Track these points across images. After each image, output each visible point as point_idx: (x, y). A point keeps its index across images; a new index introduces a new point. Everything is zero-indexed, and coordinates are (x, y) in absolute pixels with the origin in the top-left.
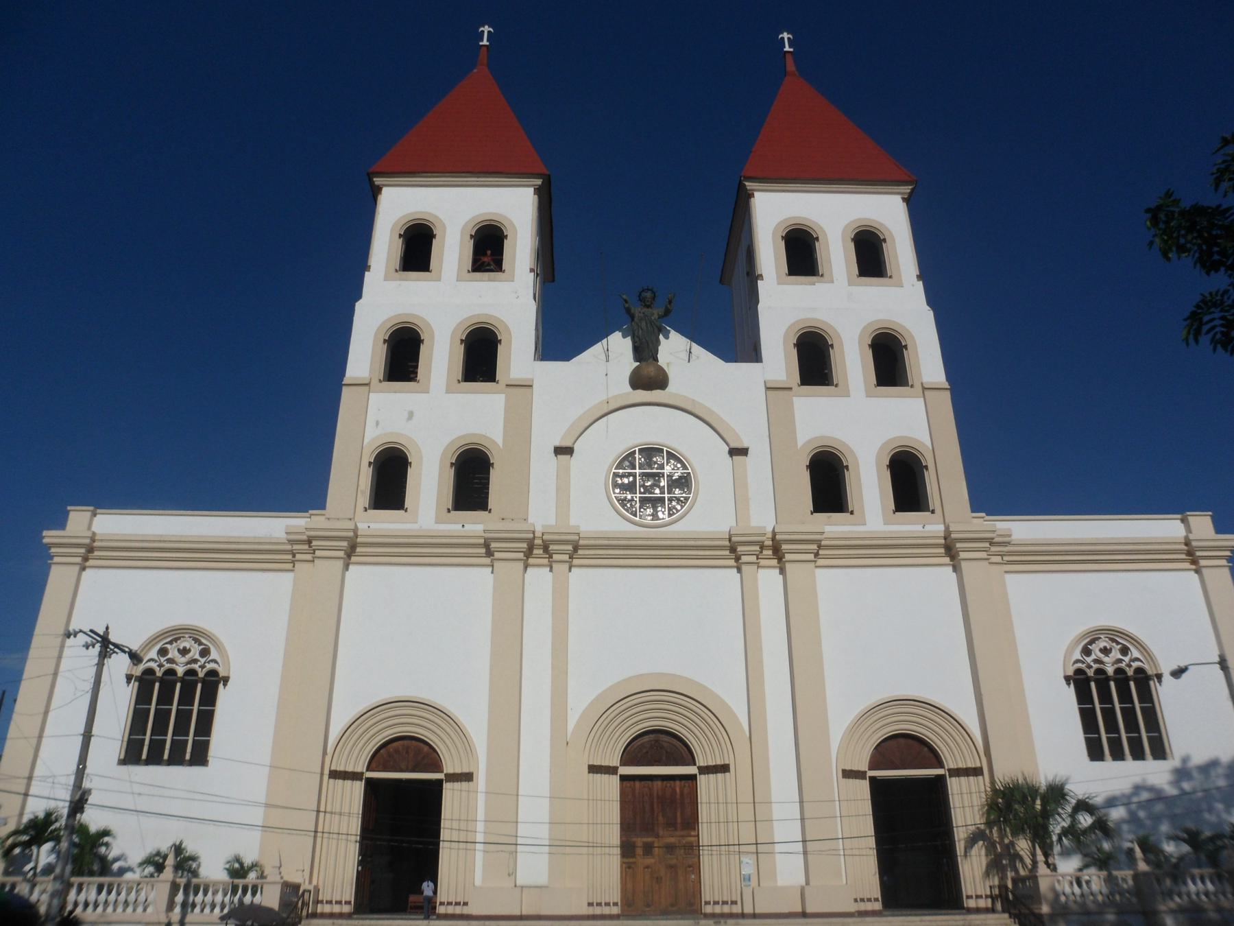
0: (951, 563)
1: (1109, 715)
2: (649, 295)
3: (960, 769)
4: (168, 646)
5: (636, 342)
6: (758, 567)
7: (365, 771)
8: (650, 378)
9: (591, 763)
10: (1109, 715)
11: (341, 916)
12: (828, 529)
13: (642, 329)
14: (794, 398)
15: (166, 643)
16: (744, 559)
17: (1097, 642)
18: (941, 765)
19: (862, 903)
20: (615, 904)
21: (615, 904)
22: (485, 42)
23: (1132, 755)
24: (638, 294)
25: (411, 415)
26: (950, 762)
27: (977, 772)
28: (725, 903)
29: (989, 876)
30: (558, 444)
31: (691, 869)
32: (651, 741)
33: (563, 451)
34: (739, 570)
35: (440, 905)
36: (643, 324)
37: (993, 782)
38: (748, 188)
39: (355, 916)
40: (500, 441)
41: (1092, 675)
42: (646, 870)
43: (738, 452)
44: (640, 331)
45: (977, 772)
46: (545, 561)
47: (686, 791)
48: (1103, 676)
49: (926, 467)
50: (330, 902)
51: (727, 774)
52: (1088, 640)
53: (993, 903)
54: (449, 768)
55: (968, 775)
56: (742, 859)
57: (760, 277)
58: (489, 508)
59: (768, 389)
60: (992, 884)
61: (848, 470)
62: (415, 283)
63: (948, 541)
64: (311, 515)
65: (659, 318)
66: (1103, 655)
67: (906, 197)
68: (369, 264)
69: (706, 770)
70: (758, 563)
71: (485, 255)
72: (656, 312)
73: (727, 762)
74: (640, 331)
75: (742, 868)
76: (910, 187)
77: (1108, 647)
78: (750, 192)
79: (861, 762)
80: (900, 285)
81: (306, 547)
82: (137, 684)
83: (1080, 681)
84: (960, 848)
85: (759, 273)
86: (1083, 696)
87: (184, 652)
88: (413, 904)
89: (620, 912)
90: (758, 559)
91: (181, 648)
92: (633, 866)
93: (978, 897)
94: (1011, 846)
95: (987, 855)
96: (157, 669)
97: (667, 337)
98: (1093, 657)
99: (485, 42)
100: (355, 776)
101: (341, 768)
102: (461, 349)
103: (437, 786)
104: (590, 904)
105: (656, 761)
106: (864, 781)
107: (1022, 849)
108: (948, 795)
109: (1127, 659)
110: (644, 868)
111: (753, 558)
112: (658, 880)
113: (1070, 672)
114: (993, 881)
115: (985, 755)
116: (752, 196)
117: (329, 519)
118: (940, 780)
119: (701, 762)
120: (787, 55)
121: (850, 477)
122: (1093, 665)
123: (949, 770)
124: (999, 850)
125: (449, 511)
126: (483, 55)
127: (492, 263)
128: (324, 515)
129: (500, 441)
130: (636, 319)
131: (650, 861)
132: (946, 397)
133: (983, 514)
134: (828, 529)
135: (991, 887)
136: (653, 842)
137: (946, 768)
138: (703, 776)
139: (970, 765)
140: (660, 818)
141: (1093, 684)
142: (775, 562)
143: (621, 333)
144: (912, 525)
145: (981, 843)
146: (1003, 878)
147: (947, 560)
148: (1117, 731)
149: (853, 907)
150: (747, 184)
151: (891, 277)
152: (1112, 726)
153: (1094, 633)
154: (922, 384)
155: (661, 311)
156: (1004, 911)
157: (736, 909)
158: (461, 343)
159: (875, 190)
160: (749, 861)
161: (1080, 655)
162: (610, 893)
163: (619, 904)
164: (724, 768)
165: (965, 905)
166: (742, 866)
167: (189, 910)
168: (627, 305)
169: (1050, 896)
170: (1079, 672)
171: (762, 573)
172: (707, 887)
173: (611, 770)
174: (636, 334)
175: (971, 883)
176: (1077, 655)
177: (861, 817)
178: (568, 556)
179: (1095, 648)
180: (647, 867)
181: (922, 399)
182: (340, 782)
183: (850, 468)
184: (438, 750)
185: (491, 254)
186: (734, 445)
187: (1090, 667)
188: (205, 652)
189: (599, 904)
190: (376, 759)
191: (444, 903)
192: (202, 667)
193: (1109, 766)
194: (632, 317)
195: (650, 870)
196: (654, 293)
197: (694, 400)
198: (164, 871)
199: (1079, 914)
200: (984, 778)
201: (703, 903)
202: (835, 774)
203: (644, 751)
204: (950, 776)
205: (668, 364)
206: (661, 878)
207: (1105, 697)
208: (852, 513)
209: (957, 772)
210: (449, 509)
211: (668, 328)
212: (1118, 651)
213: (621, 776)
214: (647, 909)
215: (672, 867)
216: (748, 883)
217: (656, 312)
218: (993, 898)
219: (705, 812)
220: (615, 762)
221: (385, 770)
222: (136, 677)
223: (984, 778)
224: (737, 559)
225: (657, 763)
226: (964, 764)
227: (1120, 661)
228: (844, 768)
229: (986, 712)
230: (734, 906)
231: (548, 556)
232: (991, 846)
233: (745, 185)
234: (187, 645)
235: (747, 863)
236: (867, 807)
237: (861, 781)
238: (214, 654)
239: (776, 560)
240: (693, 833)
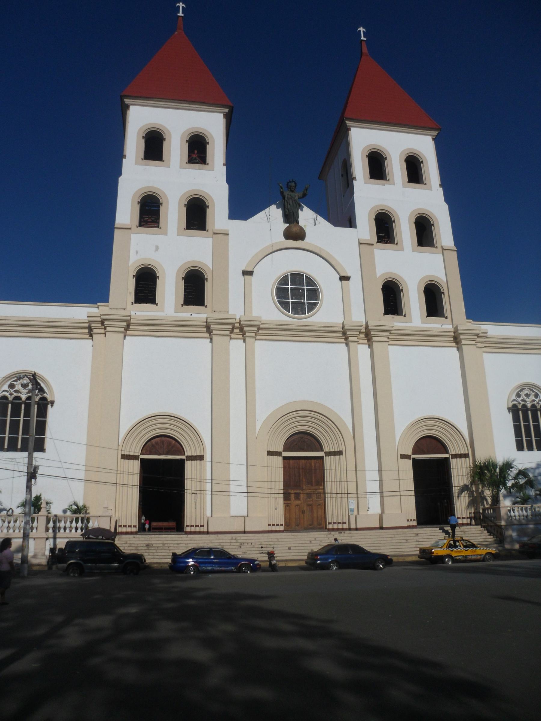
0: (368, 343)
1: (527, 428)
2: (293, 184)
3: (458, 454)
5: (286, 212)
6: (256, 340)
8: (297, 234)
9: (268, 450)
10: (527, 428)
11: (131, 533)
12: (396, 324)
13: (289, 204)
14: (375, 250)
16: (351, 339)
17: (523, 391)
18: (447, 452)
20: (282, 525)
21: (282, 525)
22: (180, 14)
23: (527, 448)
24: (286, 183)
25: (157, 248)
26: (453, 451)
27: (466, 456)
28: (339, 523)
29: (469, 508)
30: (244, 268)
31: (320, 506)
32: (298, 438)
33: (247, 273)
34: (244, 341)
35: (186, 527)
36: (291, 202)
38: (348, 125)
39: (139, 533)
41: (521, 408)
43: (344, 278)
44: (289, 206)
45: (466, 456)
46: (207, 335)
47: (317, 465)
48: (516, 408)
49: (443, 293)
51: (341, 456)
52: (519, 389)
53: (471, 520)
54: (189, 452)
55: (335, 455)
56: (349, 501)
57: (354, 178)
58: (156, 303)
59: (360, 244)
60: (470, 512)
62: (153, 167)
63: (456, 334)
64: (98, 306)
65: (298, 199)
66: (526, 398)
67: (434, 137)
68: (124, 154)
70: (256, 337)
71: (194, 153)
72: (297, 195)
73: (341, 450)
74: (289, 206)
75: (349, 505)
76: (437, 132)
77: (529, 394)
78: (348, 127)
79: (136, 450)
80: (431, 189)
81: (100, 325)
83: (514, 410)
84: (455, 494)
85: (354, 176)
86: (516, 419)
88: (153, 527)
89: (284, 529)
90: (256, 335)
92: (289, 505)
93: (463, 518)
94: (482, 493)
95: (469, 496)
97: (302, 210)
98: (521, 398)
99: (180, 14)
101: (127, 453)
102: (185, 210)
103: (182, 462)
104: (269, 525)
105: (301, 449)
106: (137, 461)
107: (487, 494)
108: (451, 469)
109: (537, 400)
110: (295, 506)
111: (253, 334)
112: (303, 512)
113: (510, 406)
114: (471, 511)
115: (470, 447)
116: (349, 129)
117: (111, 309)
118: (447, 460)
120: (362, 42)
121: (403, 296)
122: (521, 403)
123: (451, 455)
124: (475, 495)
125: (182, 306)
126: (180, 22)
127: (198, 158)
128: (108, 306)
130: (286, 198)
131: (298, 502)
132: (455, 254)
133: (471, 321)
134: (396, 324)
135: (470, 513)
136: (300, 492)
137: (450, 454)
138: (327, 457)
139: (463, 452)
140: (304, 480)
142: (365, 341)
143: (276, 206)
145: (466, 491)
146: (476, 509)
147: (454, 344)
148: (531, 436)
149: (406, 524)
150: (347, 122)
151: (425, 184)
152: (528, 434)
153: (522, 386)
154: (442, 246)
155: (300, 195)
156: (476, 525)
157: (202, 529)
158: (138, 204)
159: (422, 133)
161: (515, 397)
163: (283, 525)
164: (340, 453)
166: (349, 504)
167: (58, 531)
168: (282, 190)
169: (505, 517)
170: (514, 406)
171: (360, 346)
172: (330, 516)
173: (278, 454)
174: (286, 207)
175: (460, 511)
176: (514, 397)
177: (408, 480)
178: (123, 328)
179: (523, 394)
180: (297, 506)
181: (442, 255)
182: (127, 461)
184: (181, 443)
185: (197, 153)
186: (343, 274)
187: (520, 403)
189: (274, 525)
190: (144, 448)
191: (189, 526)
193: (526, 453)
194: (284, 198)
195: (298, 507)
196: (295, 183)
197: (320, 247)
198: (41, 510)
199: (518, 525)
200: (469, 460)
201: (327, 524)
203: (295, 443)
205: (305, 226)
206: (305, 511)
207: (526, 419)
208: (405, 316)
209: (456, 456)
210: (182, 305)
211: (303, 205)
212: (533, 396)
213: (283, 457)
214: (297, 527)
215: (309, 505)
216: (352, 513)
217: (297, 195)
218: (471, 518)
219: (328, 475)
220: (280, 449)
221: (150, 454)
223: (469, 460)
224: (244, 335)
225: (302, 450)
226: (459, 452)
227: (534, 401)
228: (401, 453)
229: (473, 424)
230: (344, 525)
231: (242, 333)
232: (471, 494)
233: (346, 123)
236: (410, 474)
237: (408, 460)
239: (366, 340)
240: (321, 488)
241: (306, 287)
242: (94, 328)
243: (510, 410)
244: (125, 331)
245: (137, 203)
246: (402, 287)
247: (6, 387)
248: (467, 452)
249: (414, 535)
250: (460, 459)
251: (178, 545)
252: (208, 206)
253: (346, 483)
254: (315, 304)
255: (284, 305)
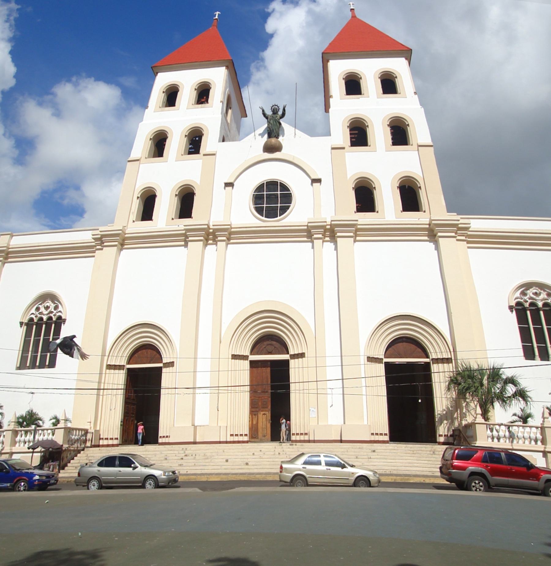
4: (40, 306)
7: (125, 364)
9: (233, 353)
15: (40, 304)
18: (427, 357)
19: (377, 436)
20: (246, 435)
21: (246, 435)
27: (448, 361)
37: (456, 367)
40: (198, 182)
41: (528, 306)
42: (264, 416)
45: (448, 361)
49: (420, 187)
50: (107, 439)
51: (304, 359)
55: (443, 363)
57: (331, 97)
61: (375, 190)
69: (294, 356)
73: (304, 352)
79: (380, 353)
82: (25, 327)
86: (28, 334)
87: (47, 308)
89: (248, 440)
91: (46, 306)
96: (35, 318)
98: (528, 296)
100: (120, 367)
104: (372, 434)
106: (381, 364)
113: (513, 303)
118: (427, 365)
119: (292, 352)
123: (432, 359)
125: (402, 212)
129: (198, 182)
137: (431, 358)
139: (445, 356)
141: (528, 313)
144: (412, 218)
154: (417, 144)
160: (314, 410)
162: (244, 430)
165: (438, 441)
170: (518, 304)
173: (245, 358)
176: (518, 294)
183: (376, 188)
188: (56, 308)
189: (237, 435)
192: (55, 315)
195: (265, 416)
200: (107, 362)
202: (363, 360)
204: (433, 363)
207: (537, 320)
209: (437, 361)
214: (264, 438)
220: (247, 352)
222: (25, 323)
230: (306, 436)
234: (48, 304)
235: (313, 411)
238: (60, 308)
241: (280, 191)
242: (219, 235)
243: (512, 309)
244: (323, 237)
245: (347, 127)
246: (376, 185)
247: (33, 310)
248: (450, 357)
249: (370, 451)
250: (437, 364)
251: (369, 456)
252: (368, 126)
253: (220, 388)
254: (288, 208)
255: (259, 210)
